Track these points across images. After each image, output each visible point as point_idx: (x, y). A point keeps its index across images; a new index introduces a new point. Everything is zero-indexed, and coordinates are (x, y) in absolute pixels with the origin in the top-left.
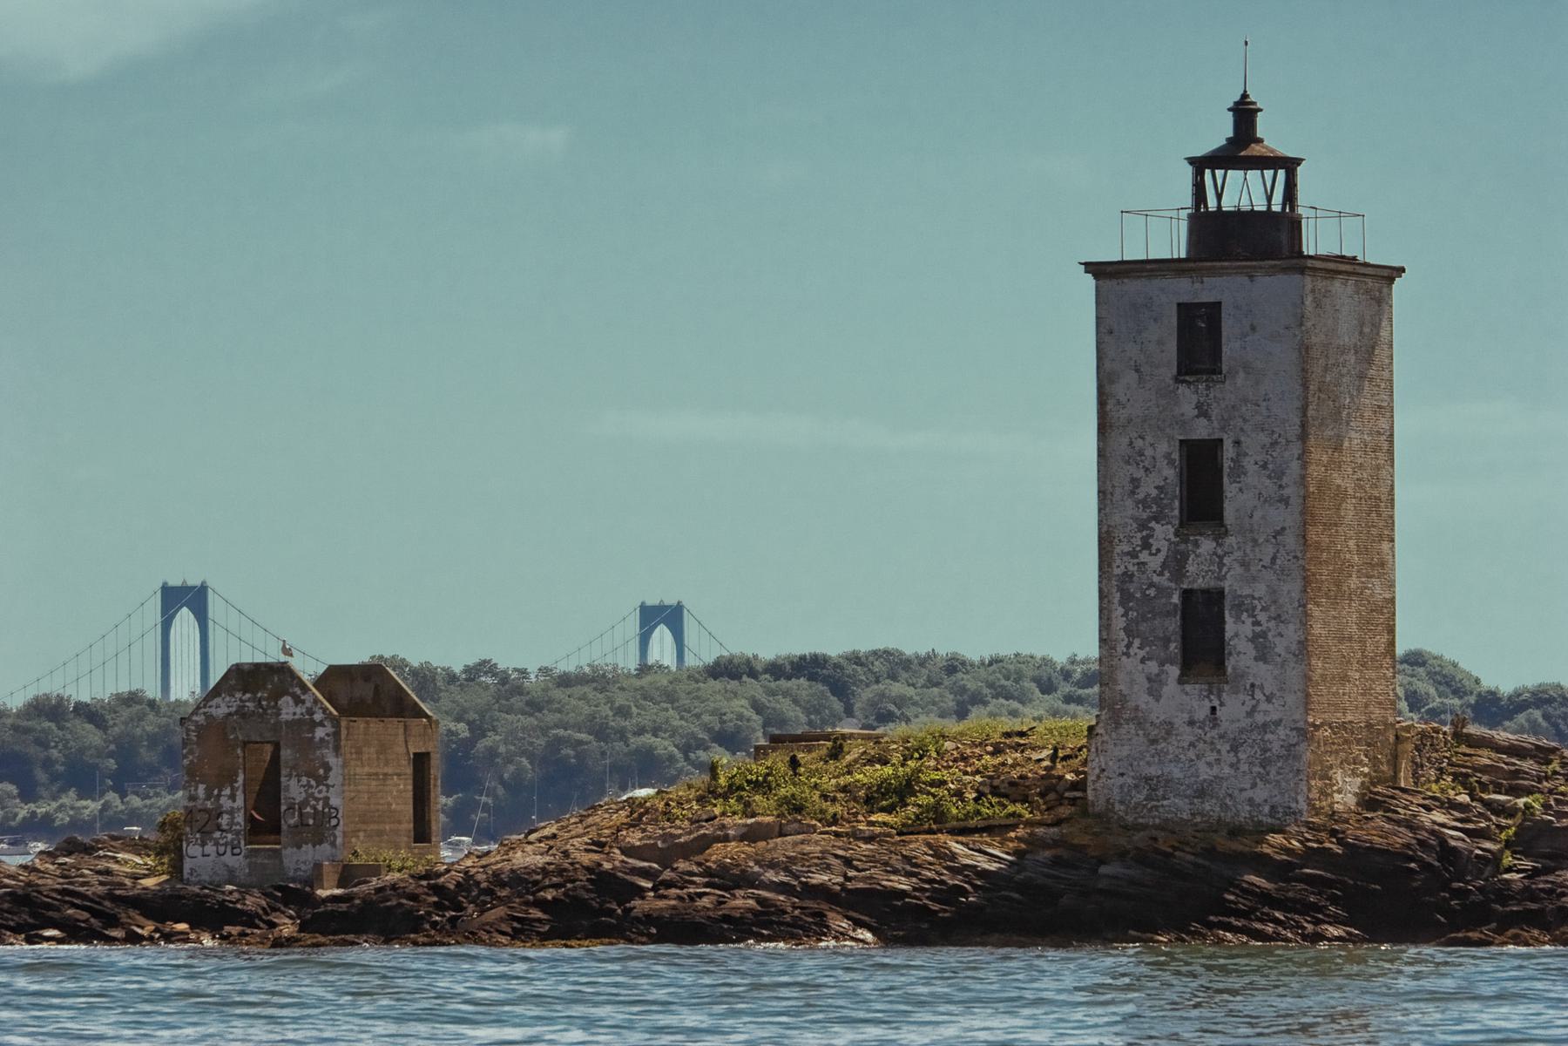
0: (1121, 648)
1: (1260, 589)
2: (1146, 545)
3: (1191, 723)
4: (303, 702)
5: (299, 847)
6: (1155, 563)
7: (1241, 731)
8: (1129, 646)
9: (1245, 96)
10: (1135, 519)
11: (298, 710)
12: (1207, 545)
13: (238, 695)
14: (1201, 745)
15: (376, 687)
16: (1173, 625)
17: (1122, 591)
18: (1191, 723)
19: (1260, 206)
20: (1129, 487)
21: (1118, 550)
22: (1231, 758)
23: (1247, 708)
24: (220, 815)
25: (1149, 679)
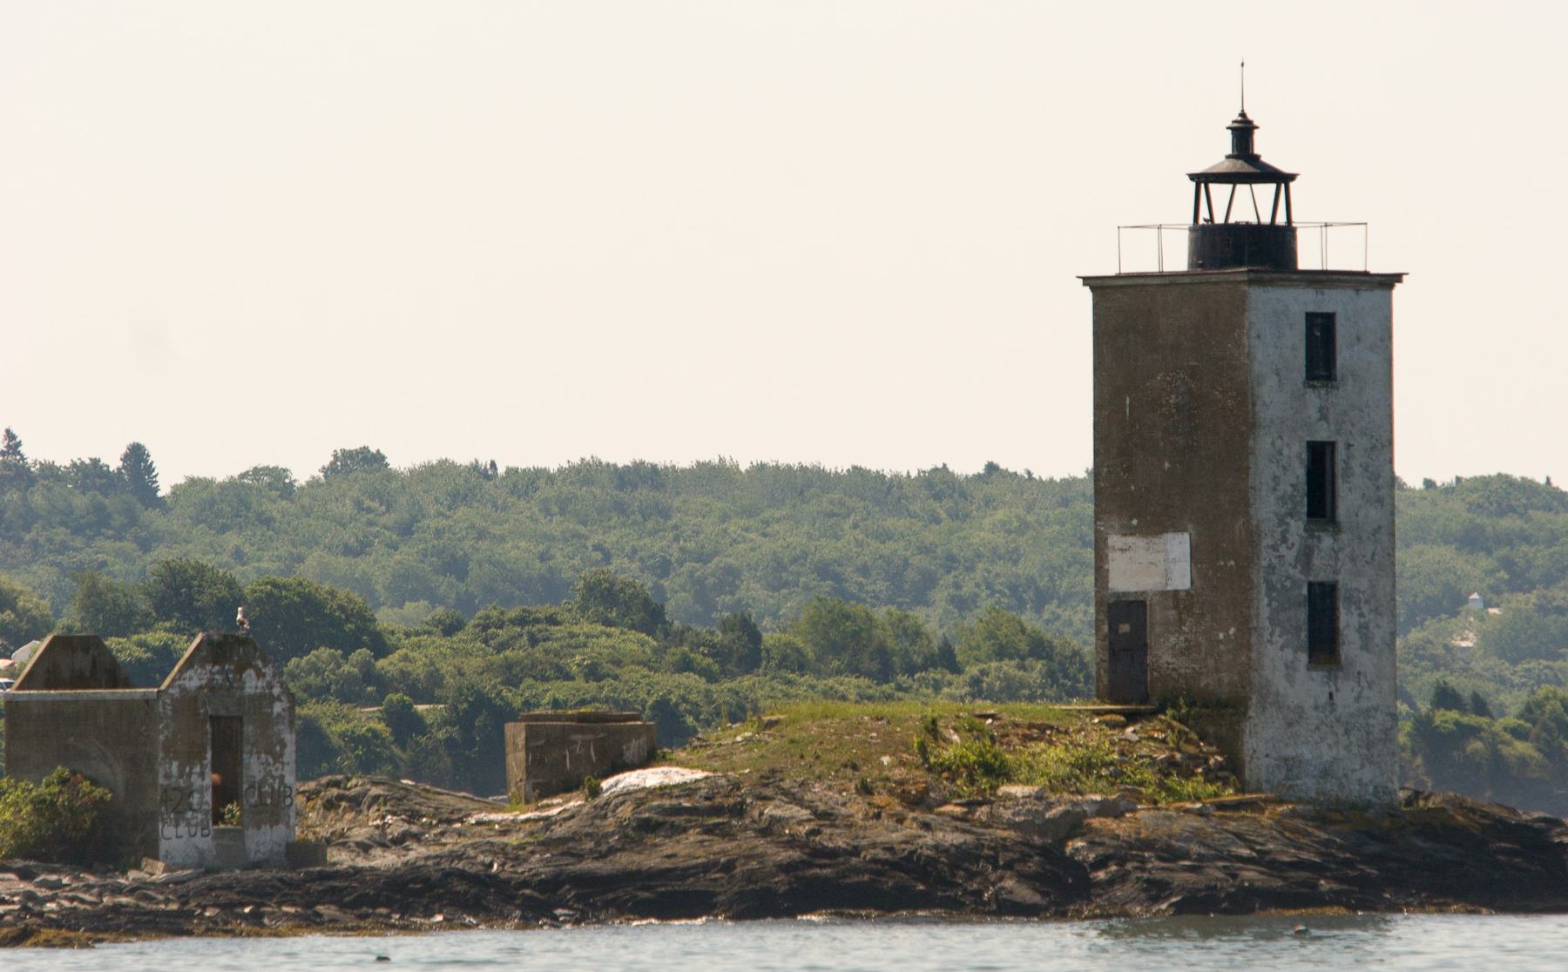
0: (1267, 636)
1: (1364, 584)
2: (1284, 540)
3: (1316, 708)
4: (264, 675)
5: (259, 828)
6: (1290, 555)
7: (1352, 715)
8: (1272, 635)
9: (1243, 115)
10: (1276, 514)
11: (260, 684)
12: (1327, 541)
13: (208, 667)
14: (1323, 728)
15: (94, 662)
16: (1302, 615)
17: (1267, 581)
18: (1316, 708)
19: (1266, 219)
20: (1272, 484)
21: (1264, 543)
22: (1344, 740)
23: (1355, 694)
24: (191, 793)
25: (1287, 667)
